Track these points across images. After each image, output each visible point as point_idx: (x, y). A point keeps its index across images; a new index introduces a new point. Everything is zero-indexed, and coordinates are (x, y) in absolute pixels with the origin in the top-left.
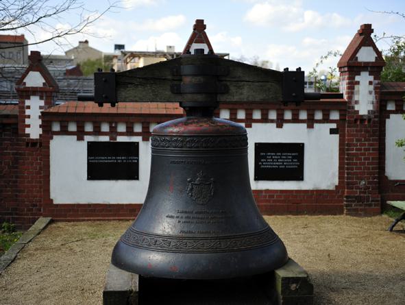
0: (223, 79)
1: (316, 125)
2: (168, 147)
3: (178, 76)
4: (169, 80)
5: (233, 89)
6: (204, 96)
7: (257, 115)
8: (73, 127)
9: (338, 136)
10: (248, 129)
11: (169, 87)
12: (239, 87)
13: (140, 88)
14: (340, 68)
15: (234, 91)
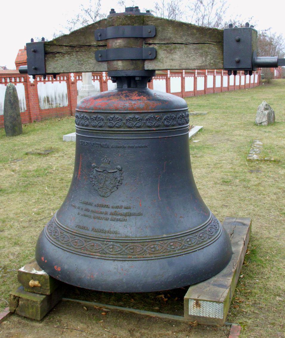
0: (151, 42)
1: (61, 82)
2: (120, 127)
3: (104, 40)
4: (93, 46)
5: (162, 54)
6: (126, 63)
7: (18, 80)
8: (206, 212)
9: (186, 91)
10: (15, 86)
11: (94, 55)
12: (170, 52)
13: (67, 57)
14: (16, 64)
15: (163, 56)
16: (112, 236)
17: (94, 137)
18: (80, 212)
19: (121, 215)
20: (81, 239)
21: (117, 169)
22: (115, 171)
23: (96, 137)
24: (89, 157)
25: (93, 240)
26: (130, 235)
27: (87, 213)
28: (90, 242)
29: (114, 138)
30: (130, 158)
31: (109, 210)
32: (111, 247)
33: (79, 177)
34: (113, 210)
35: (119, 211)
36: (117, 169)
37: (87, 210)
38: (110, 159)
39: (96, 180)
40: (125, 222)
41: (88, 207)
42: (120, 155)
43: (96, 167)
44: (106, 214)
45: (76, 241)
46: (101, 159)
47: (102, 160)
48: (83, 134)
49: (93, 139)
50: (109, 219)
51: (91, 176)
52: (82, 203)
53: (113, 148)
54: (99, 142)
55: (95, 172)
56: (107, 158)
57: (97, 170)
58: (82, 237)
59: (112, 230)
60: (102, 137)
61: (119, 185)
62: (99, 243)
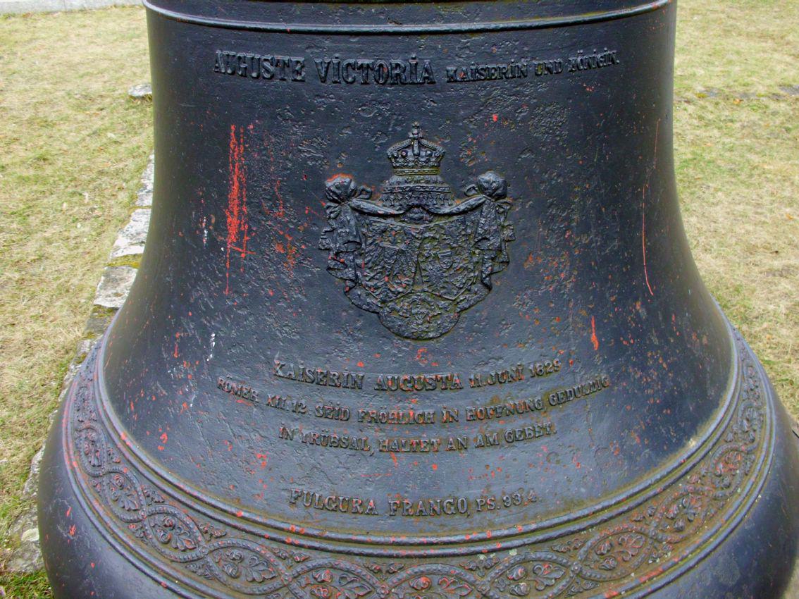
16: (503, 524)
17: (330, 28)
18: (295, 426)
19: (529, 409)
20: (344, 563)
21: (481, 189)
22: (472, 201)
23: (345, 28)
24: (298, 143)
25: (415, 561)
26: (583, 490)
27: (336, 430)
28: (403, 575)
29: (465, 27)
30: (543, 129)
31: (461, 404)
32: (519, 571)
33: (239, 244)
34: (482, 399)
35: (511, 396)
36: (481, 189)
37: (338, 415)
38: (443, 145)
39: (359, 261)
40: (546, 439)
41: (336, 400)
42: (495, 117)
43: (354, 193)
44: (452, 419)
45: (323, 575)
46: (388, 145)
47: (391, 150)
48: (238, 18)
49: (327, 43)
50: (472, 445)
51: (327, 242)
52: (289, 378)
53: (460, 85)
54: (365, 56)
55: (349, 216)
56: (424, 142)
57: (366, 205)
58: (349, 553)
59: (496, 490)
60: (391, 27)
61: (496, 268)
62: (454, 567)
